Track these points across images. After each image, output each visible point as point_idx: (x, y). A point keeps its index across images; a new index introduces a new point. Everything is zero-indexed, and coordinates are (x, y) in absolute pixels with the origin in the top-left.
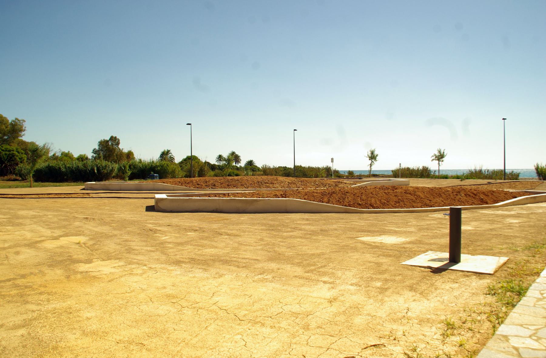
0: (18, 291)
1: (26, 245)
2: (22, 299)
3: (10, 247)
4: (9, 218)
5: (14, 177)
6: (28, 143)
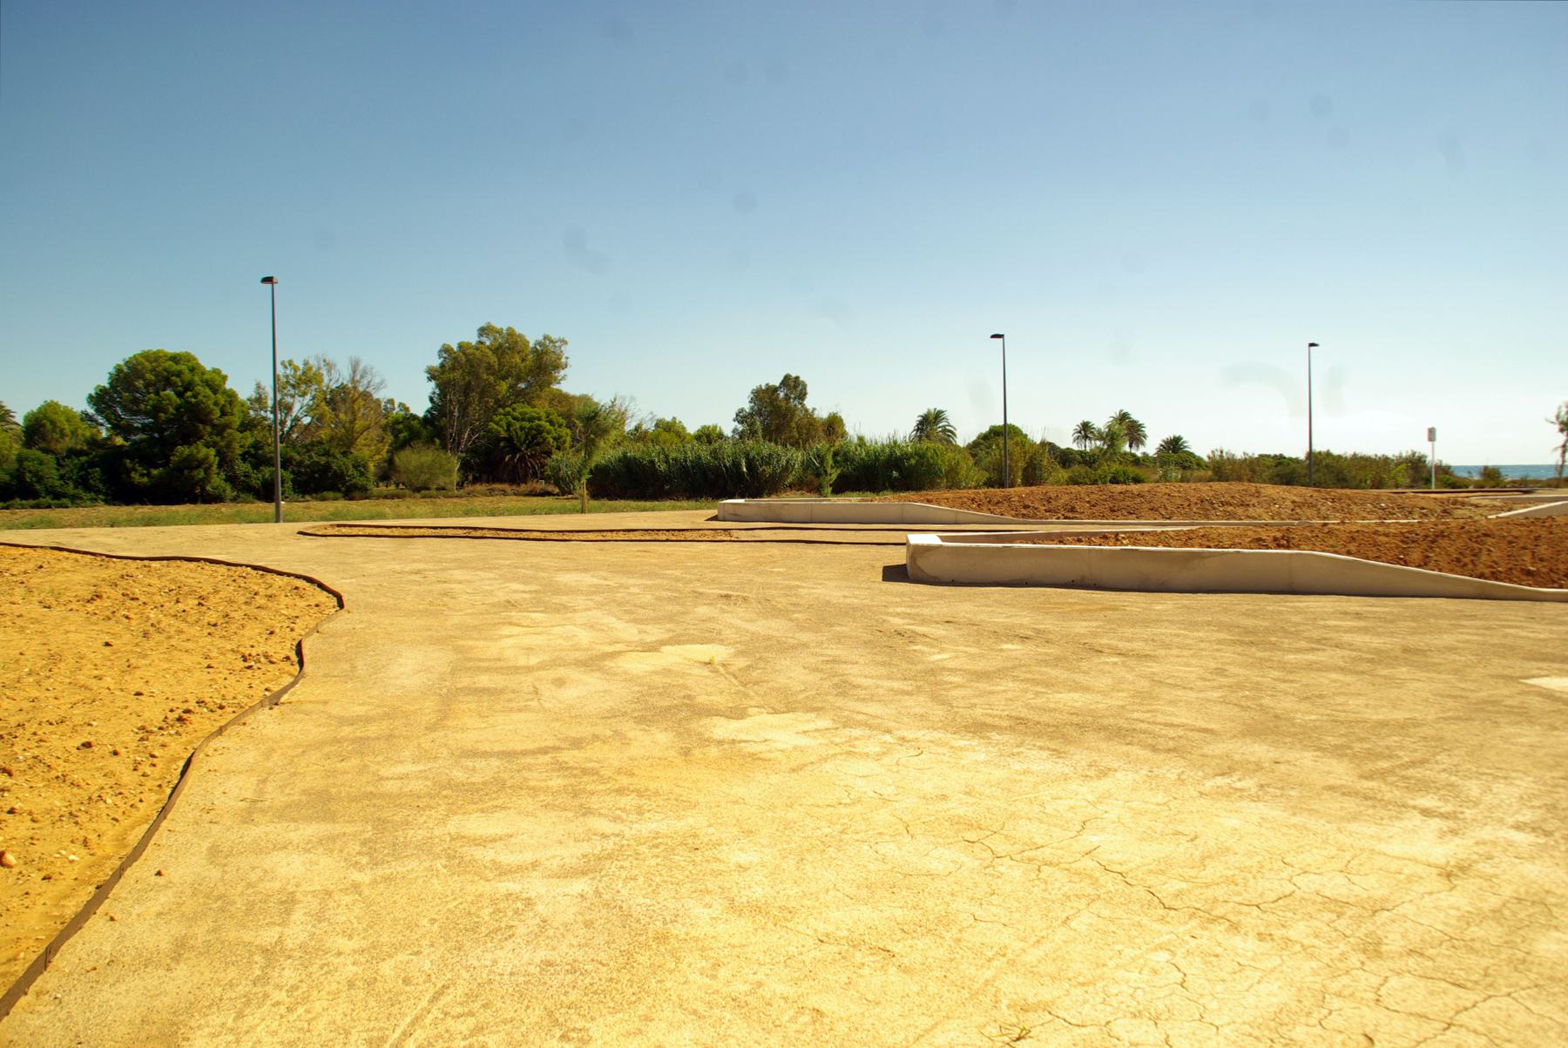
2: (576, 803)
3: (542, 666)
5: (541, 485)
6: (574, 397)
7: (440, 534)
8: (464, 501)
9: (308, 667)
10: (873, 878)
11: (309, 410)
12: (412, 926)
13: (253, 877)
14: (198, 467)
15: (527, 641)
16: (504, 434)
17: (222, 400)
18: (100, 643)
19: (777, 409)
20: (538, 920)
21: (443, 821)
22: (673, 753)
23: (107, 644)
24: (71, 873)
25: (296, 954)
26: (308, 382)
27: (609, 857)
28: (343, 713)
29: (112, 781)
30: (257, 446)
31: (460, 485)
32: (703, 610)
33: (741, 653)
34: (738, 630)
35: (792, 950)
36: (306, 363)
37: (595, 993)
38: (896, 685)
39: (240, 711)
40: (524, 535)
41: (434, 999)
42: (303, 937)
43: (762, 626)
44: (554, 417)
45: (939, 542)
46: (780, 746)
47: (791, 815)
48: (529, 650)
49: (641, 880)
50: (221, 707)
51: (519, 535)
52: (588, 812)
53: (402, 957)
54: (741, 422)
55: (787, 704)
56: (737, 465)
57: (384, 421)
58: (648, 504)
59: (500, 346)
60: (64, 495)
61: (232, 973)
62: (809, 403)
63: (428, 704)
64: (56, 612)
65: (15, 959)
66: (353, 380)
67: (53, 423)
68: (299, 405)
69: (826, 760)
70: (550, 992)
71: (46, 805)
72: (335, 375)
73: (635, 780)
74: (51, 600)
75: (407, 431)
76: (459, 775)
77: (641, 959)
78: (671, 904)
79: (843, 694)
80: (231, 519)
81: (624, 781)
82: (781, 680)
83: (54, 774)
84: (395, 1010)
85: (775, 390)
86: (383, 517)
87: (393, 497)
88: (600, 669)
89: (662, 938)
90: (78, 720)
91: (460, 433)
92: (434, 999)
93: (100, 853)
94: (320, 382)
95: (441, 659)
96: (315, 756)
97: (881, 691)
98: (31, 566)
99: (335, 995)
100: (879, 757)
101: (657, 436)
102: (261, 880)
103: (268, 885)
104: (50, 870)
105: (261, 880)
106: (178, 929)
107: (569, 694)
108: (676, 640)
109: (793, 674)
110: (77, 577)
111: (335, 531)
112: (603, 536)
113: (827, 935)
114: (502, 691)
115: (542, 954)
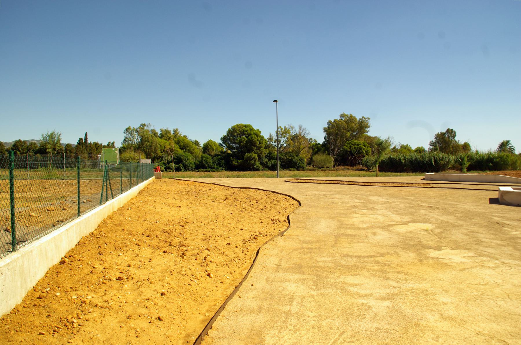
2: (383, 275)
3: (368, 228)
5: (361, 167)
6: (372, 137)
7: (330, 182)
8: (335, 172)
10: (496, 313)
11: (286, 142)
12: (331, 311)
13: (280, 289)
14: (252, 160)
16: (349, 150)
18: (229, 213)
19: (445, 141)
20: (373, 314)
21: (339, 277)
22: (416, 261)
23: (231, 214)
24: (228, 282)
25: (295, 315)
26: (286, 133)
27: (396, 294)
29: (237, 256)
30: (270, 153)
31: (334, 167)
32: (422, 211)
33: (438, 227)
34: (436, 219)
35: (466, 336)
36: (285, 127)
37: (395, 341)
38: (499, 242)
39: (272, 237)
40: (357, 183)
41: (340, 335)
42: (297, 310)
43: (444, 218)
44: (366, 144)
45: (512, 190)
46: (455, 261)
47: (461, 286)
48: (363, 222)
49: (408, 304)
50: (266, 235)
52: (388, 278)
53: (329, 320)
54: (432, 145)
55: (456, 246)
56: (430, 161)
58: (398, 174)
59: (348, 120)
60: (214, 168)
61: (276, 319)
62: (457, 139)
63: (331, 238)
64: (216, 203)
65: (215, 305)
66: (300, 132)
68: (283, 140)
69: (473, 267)
70: (379, 338)
71: (220, 261)
72: (294, 131)
73: (403, 269)
74: (214, 199)
76: (343, 262)
77: (410, 331)
78: (419, 313)
79: (478, 244)
80: (262, 176)
81: (400, 269)
82: (454, 238)
83: (221, 252)
84: (328, 337)
85: (444, 134)
86: (309, 176)
88: (388, 230)
89: (417, 325)
90: (226, 236)
91: (334, 149)
92: (340, 335)
93: (235, 277)
94: (289, 133)
95: (334, 224)
96: (296, 253)
97: (493, 244)
98: (208, 189)
100: (494, 268)
101: (401, 151)
103: (285, 292)
104: (223, 280)
106: (260, 303)
107: (378, 238)
108: (414, 222)
109: (458, 235)
110: (221, 193)
111: (296, 181)
112: (384, 184)
113: (480, 332)
114: (355, 236)
115: (375, 325)
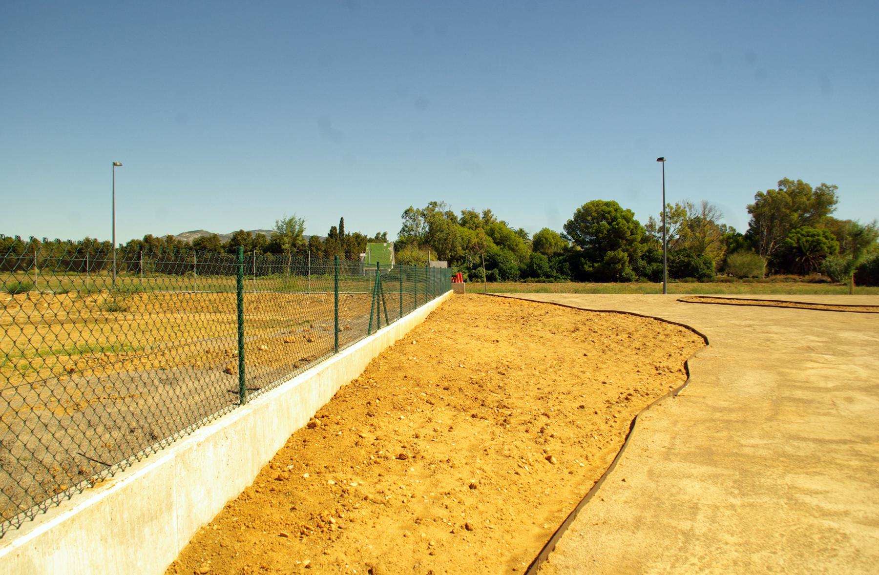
0: (862, 464)
1: (861, 389)
2: (871, 478)
3: (836, 389)
4: (826, 342)
5: (819, 276)
6: (842, 222)
9: (692, 377)
11: (679, 231)
12: (769, 536)
13: (674, 490)
14: (618, 262)
15: (825, 372)
16: (795, 245)
17: (631, 226)
18: (581, 355)
21: (783, 476)
23: (585, 355)
24: (582, 472)
26: (678, 215)
28: (715, 405)
29: (596, 428)
30: (650, 251)
31: (767, 275)
36: (677, 205)
39: (657, 398)
40: (813, 307)
42: (704, 530)
48: (826, 378)
50: (647, 394)
51: (810, 306)
57: (722, 237)
61: (667, 542)
63: (765, 404)
64: (558, 337)
66: (704, 214)
67: (546, 239)
68: (673, 229)
72: (694, 211)
74: (555, 330)
75: (734, 243)
76: (789, 449)
80: (637, 291)
83: (568, 420)
87: (726, 281)
90: (576, 393)
91: (768, 244)
94: (685, 215)
95: (770, 379)
96: (701, 427)
98: (543, 312)
99: (726, 567)
102: (678, 493)
103: (683, 497)
104: (574, 469)
105: (678, 493)
106: (637, 512)
110: (566, 319)
111: (698, 300)
